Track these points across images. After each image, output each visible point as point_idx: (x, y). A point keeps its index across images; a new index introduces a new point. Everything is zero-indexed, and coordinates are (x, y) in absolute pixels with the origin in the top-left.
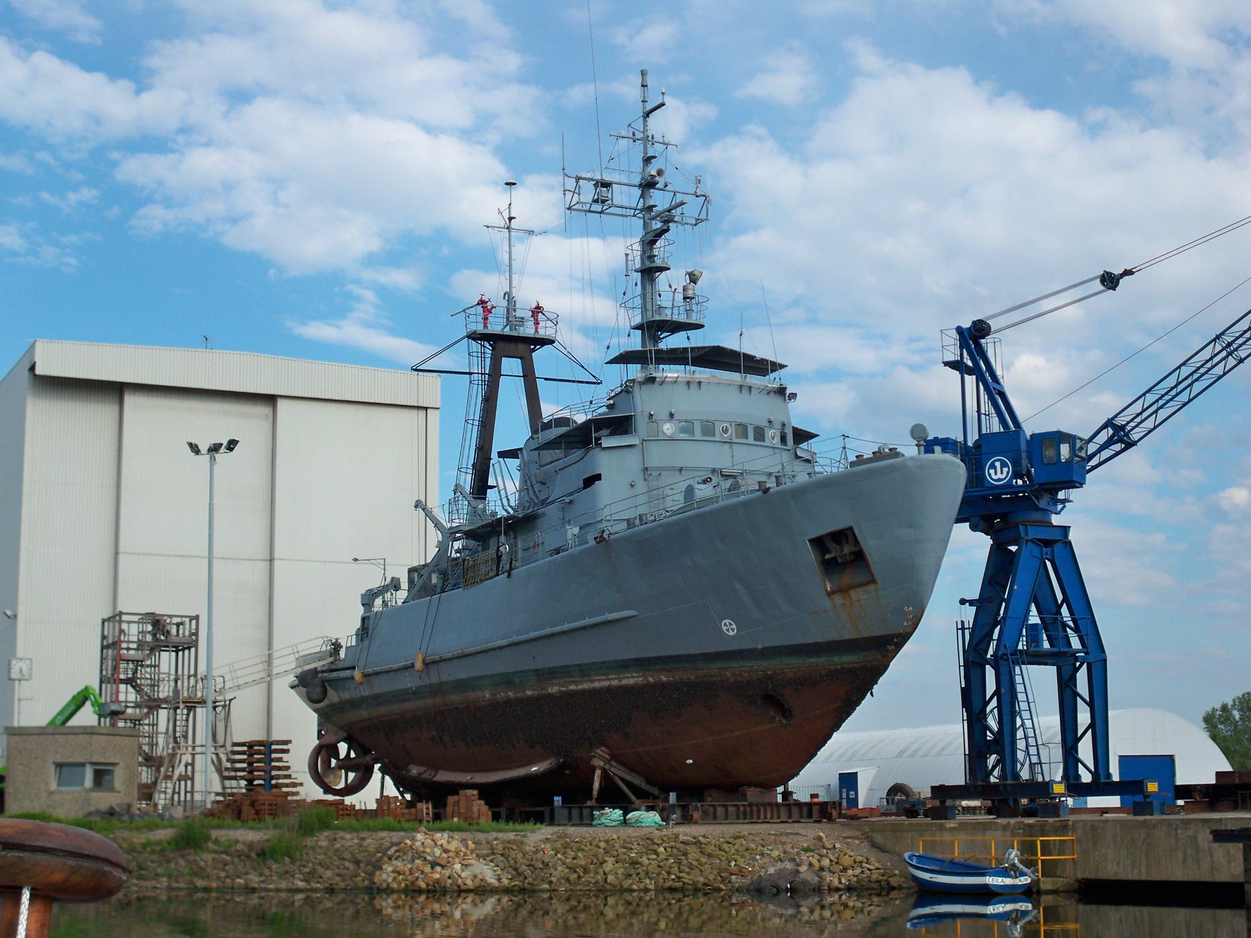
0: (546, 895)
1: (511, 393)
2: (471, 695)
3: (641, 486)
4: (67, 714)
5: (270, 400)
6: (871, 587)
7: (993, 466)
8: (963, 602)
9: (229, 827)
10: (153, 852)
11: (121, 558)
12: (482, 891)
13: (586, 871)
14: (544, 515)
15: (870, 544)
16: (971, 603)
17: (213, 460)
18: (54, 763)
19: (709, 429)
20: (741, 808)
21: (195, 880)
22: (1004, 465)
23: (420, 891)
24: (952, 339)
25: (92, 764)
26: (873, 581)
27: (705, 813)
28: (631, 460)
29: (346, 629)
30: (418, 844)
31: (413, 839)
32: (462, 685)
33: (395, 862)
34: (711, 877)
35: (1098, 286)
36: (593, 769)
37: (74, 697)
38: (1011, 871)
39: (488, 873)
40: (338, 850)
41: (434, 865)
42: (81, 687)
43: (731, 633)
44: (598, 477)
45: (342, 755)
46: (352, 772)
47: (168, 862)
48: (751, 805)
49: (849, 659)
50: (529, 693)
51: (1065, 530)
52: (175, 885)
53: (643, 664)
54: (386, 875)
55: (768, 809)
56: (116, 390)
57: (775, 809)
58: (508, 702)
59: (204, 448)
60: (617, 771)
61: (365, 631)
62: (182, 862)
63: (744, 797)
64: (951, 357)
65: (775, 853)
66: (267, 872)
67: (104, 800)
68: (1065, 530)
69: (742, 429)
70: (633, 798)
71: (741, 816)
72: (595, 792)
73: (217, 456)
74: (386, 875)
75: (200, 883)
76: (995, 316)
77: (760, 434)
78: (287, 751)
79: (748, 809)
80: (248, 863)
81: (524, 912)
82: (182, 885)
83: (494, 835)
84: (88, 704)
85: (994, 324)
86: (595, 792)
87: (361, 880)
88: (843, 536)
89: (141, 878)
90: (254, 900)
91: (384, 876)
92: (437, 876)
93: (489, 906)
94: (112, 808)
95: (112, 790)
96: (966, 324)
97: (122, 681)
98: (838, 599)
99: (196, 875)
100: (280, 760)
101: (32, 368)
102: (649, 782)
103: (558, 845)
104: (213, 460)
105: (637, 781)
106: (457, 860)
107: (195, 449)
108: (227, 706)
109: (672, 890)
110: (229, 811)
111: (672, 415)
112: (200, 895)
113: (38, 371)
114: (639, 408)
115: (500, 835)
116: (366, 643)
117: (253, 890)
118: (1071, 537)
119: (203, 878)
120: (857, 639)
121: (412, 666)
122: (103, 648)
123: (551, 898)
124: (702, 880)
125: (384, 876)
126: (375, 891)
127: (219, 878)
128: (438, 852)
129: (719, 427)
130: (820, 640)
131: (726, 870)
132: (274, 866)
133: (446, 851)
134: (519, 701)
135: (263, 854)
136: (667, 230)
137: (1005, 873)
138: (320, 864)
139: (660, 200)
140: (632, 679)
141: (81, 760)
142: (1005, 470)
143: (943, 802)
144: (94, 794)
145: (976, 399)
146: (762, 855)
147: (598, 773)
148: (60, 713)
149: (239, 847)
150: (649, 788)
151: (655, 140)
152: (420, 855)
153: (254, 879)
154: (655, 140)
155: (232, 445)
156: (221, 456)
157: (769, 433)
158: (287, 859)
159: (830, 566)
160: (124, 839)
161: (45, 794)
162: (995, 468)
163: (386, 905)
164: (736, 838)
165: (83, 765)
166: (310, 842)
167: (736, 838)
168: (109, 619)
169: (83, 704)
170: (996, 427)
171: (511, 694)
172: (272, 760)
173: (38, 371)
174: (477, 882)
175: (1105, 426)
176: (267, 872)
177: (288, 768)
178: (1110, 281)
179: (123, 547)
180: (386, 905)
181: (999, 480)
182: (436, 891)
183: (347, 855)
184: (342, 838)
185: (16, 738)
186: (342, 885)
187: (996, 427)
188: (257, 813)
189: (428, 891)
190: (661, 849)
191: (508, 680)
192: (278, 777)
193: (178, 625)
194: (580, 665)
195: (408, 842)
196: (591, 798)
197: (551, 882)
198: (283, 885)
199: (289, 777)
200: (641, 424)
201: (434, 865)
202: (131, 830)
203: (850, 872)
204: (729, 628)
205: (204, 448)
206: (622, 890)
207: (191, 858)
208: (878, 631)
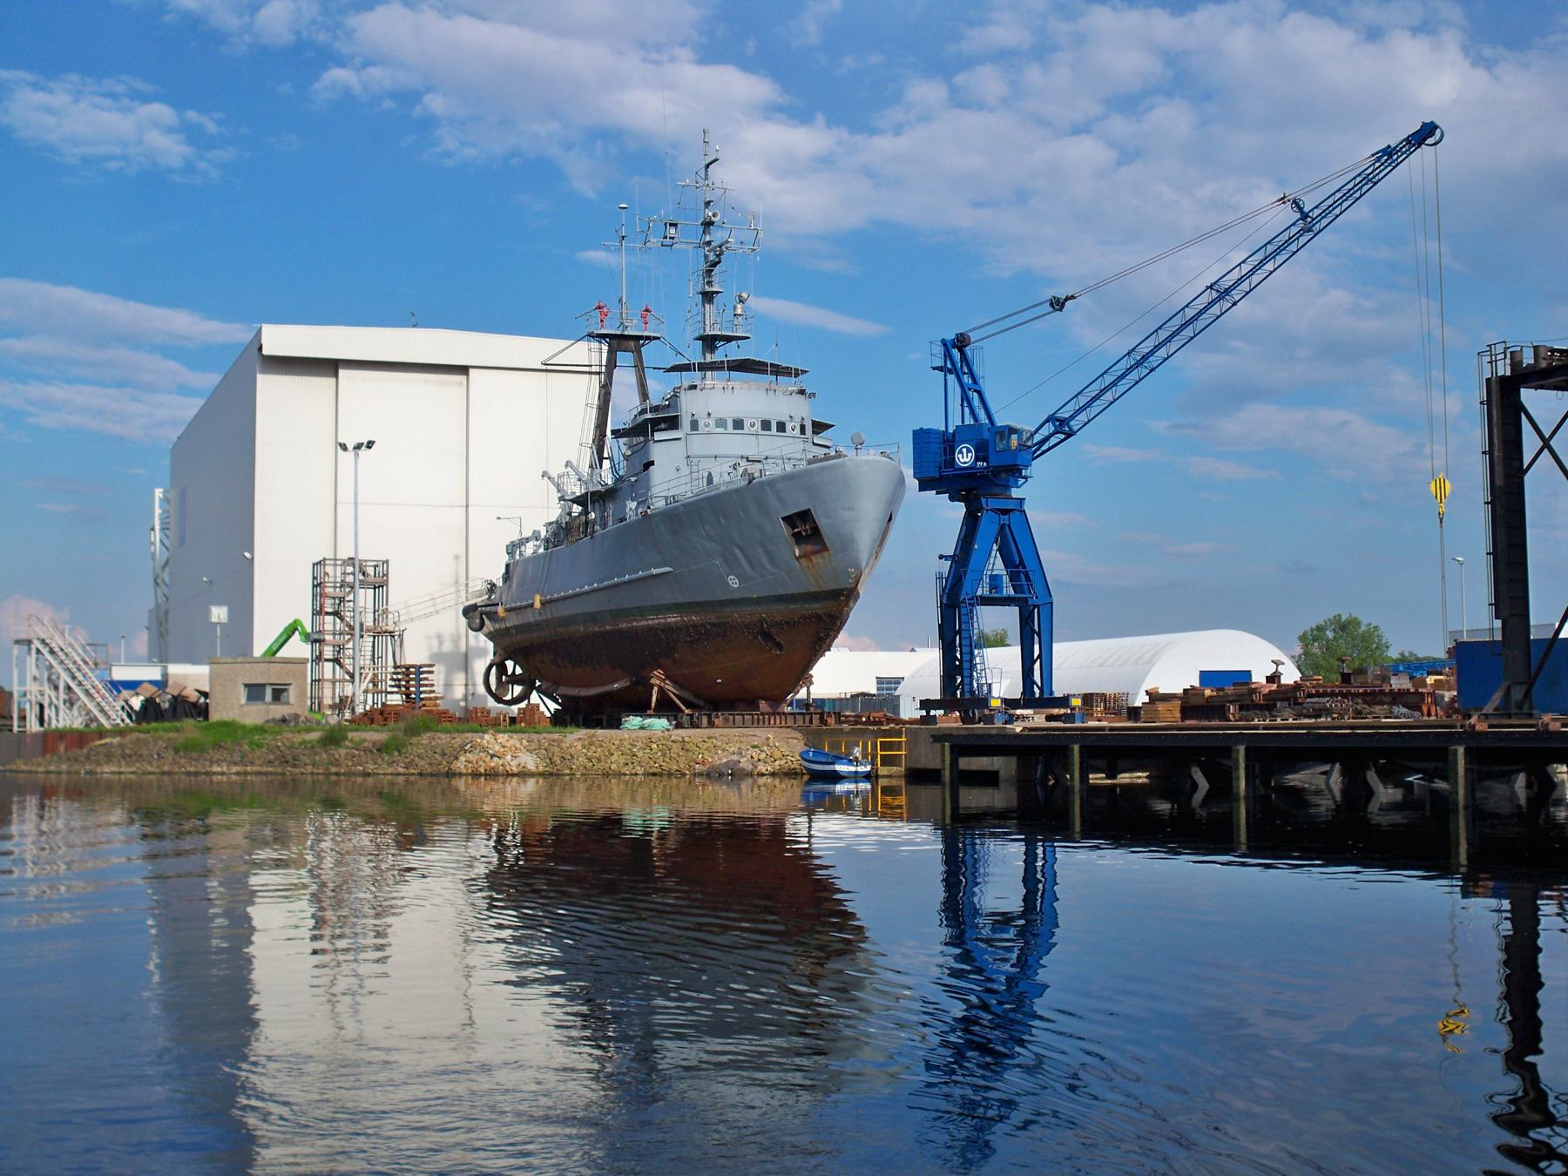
0: (567, 777)
1: (625, 378)
2: (571, 629)
3: (685, 470)
4: (281, 641)
5: (463, 370)
6: (825, 554)
7: (961, 452)
8: (941, 557)
9: (362, 731)
10: (306, 748)
11: (338, 505)
12: (523, 775)
13: (599, 760)
14: (621, 489)
15: (822, 522)
16: (946, 558)
17: (357, 455)
18: (246, 685)
19: (738, 424)
20: (756, 717)
21: (330, 767)
22: (969, 451)
23: (481, 775)
24: (939, 350)
25: (270, 684)
26: (825, 548)
27: (727, 720)
28: (678, 449)
29: (497, 576)
30: (485, 742)
31: (483, 738)
32: (570, 620)
33: (468, 755)
34: (682, 766)
35: (1047, 308)
36: (652, 686)
37: (286, 629)
38: (856, 761)
39: (530, 762)
40: (433, 746)
41: (492, 756)
42: (291, 621)
43: (735, 586)
44: (652, 463)
45: (510, 672)
46: (518, 684)
47: (315, 755)
48: (762, 714)
49: (815, 607)
50: (608, 628)
51: (1021, 500)
52: (316, 771)
53: (678, 608)
54: (460, 765)
55: (778, 717)
56: (330, 367)
57: (783, 717)
58: (595, 635)
59: (350, 447)
60: (669, 687)
61: (507, 576)
62: (324, 756)
63: (758, 708)
64: (940, 363)
65: (731, 750)
66: (379, 761)
67: (279, 711)
68: (1021, 500)
69: (766, 425)
70: (684, 708)
71: (756, 723)
72: (653, 704)
73: (360, 452)
74: (460, 765)
75: (334, 769)
76: (974, 329)
77: (781, 427)
78: (432, 672)
79: (761, 717)
80: (370, 755)
81: (557, 789)
82: (321, 771)
83: (545, 735)
84: (297, 632)
85: (973, 336)
86: (653, 704)
87: (443, 768)
88: (805, 516)
89: (295, 766)
90: (371, 780)
91: (459, 764)
92: (493, 764)
93: (531, 785)
94: (284, 716)
95: (287, 703)
96: (950, 336)
97: (328, 613)
98: (804, 562)
99: (331, 763)
100: (426, 679)
101: (260, 349)
102: (696, 696)
103: (587, 742)
104: (357, 455)
105: (686, 695)
106: (510, 753)
107: (344, 447)
108: (401, 636)
109: (654, 774)
110: (366, 718)
111: (709, 414)
112: (334, 778)
113: (265, 352)
114: (684, 409)
115: (550, 735)
116: (508, 583)
117: (369, 775)
118: (1026, 507)
119: (336, 766)
120: (819, 592)
121: (532, 605)
122: (314, 586)
123: (571, 780)
124: (675, 767)
125: (459, 764)
126: (451, 775)
127: (347, 766)
128: (497, 748)
129: (747, 424)
130: (795, 592)
131: (694, 760)
132: (386, 758)
133: (503, 747)
134: (602, 634)
135: (381, 749)
136: (719, 262)
137: (850, 762)
138: (418, 756)
139: (716, 236)
140: (673, 619)
141: (262, 682)
142: (970, 455)
143: (928, 712)
144: (272, 707)
145: (949, 403)
146: (723, 750)
147: (656, 689)
148: (276, 641)
149: (366, 745)
150: (696, 701)
151: (716, 186)
152: (484, 749)
153: (371, 767)
154: (716, 186)
155: (370, 444)
156: (363, 452)
157: (789, 427)
158: (396, 753)
159: (798, 538)
160: (288, 739)
161: (237, 707)
162: (962, 453)
163: (461, 784)
164: (709, 738)
165: (264, 685)
166: (414, 740)
167: (709, 738)
168: (317, 564)
169: (294, 633)
170: (969, 421)
171: (597, 629)
172: (421, 680)
173: (265, 352)
174: (520, 769)
175: (1047, 421)
176: (379, 761)
177: (432, 685)
178: (1058, 304)
179: (339, 500)
180: (461, 784)
181: (965, 463)
182: (492, 775)
183: (438, 750)
184: (439, 738)
185: (216, 666)
186: (429, 771)
187: (969, 421)
188: (385, 720)
189: (486, 775)
190: (654, 746)
191: (593, 617)
192: (425, 692)
193: (375, 567)
194: (639, 607)
195: (479, 740)
196: (650, 709)
197: (572, 769)
198: (390, 770)
199: (433, 692)
200: (686, 422)
201: (492, 756)
202: (293, 733)
203: (777, 763)
204: (733, 582)
205: (350, 447)
206: (620, 774)
207: (331, 752)
208: (832, 586)
